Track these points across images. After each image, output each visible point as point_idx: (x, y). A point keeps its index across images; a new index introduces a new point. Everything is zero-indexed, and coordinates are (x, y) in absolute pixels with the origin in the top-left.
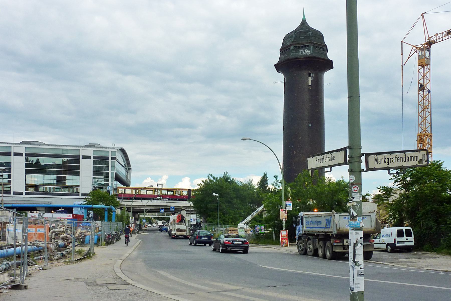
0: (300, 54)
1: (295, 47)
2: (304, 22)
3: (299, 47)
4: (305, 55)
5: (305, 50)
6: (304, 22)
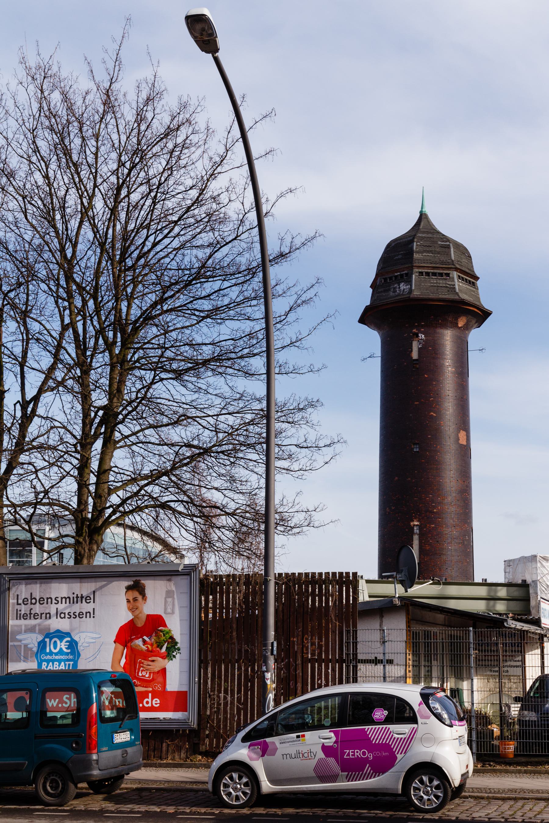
0: (391, 294)
1: (385, 279)
2: (423, 216)
3: (391, 278)
4: (399, 295)
5: (402, 285)
6: (423, 216)
